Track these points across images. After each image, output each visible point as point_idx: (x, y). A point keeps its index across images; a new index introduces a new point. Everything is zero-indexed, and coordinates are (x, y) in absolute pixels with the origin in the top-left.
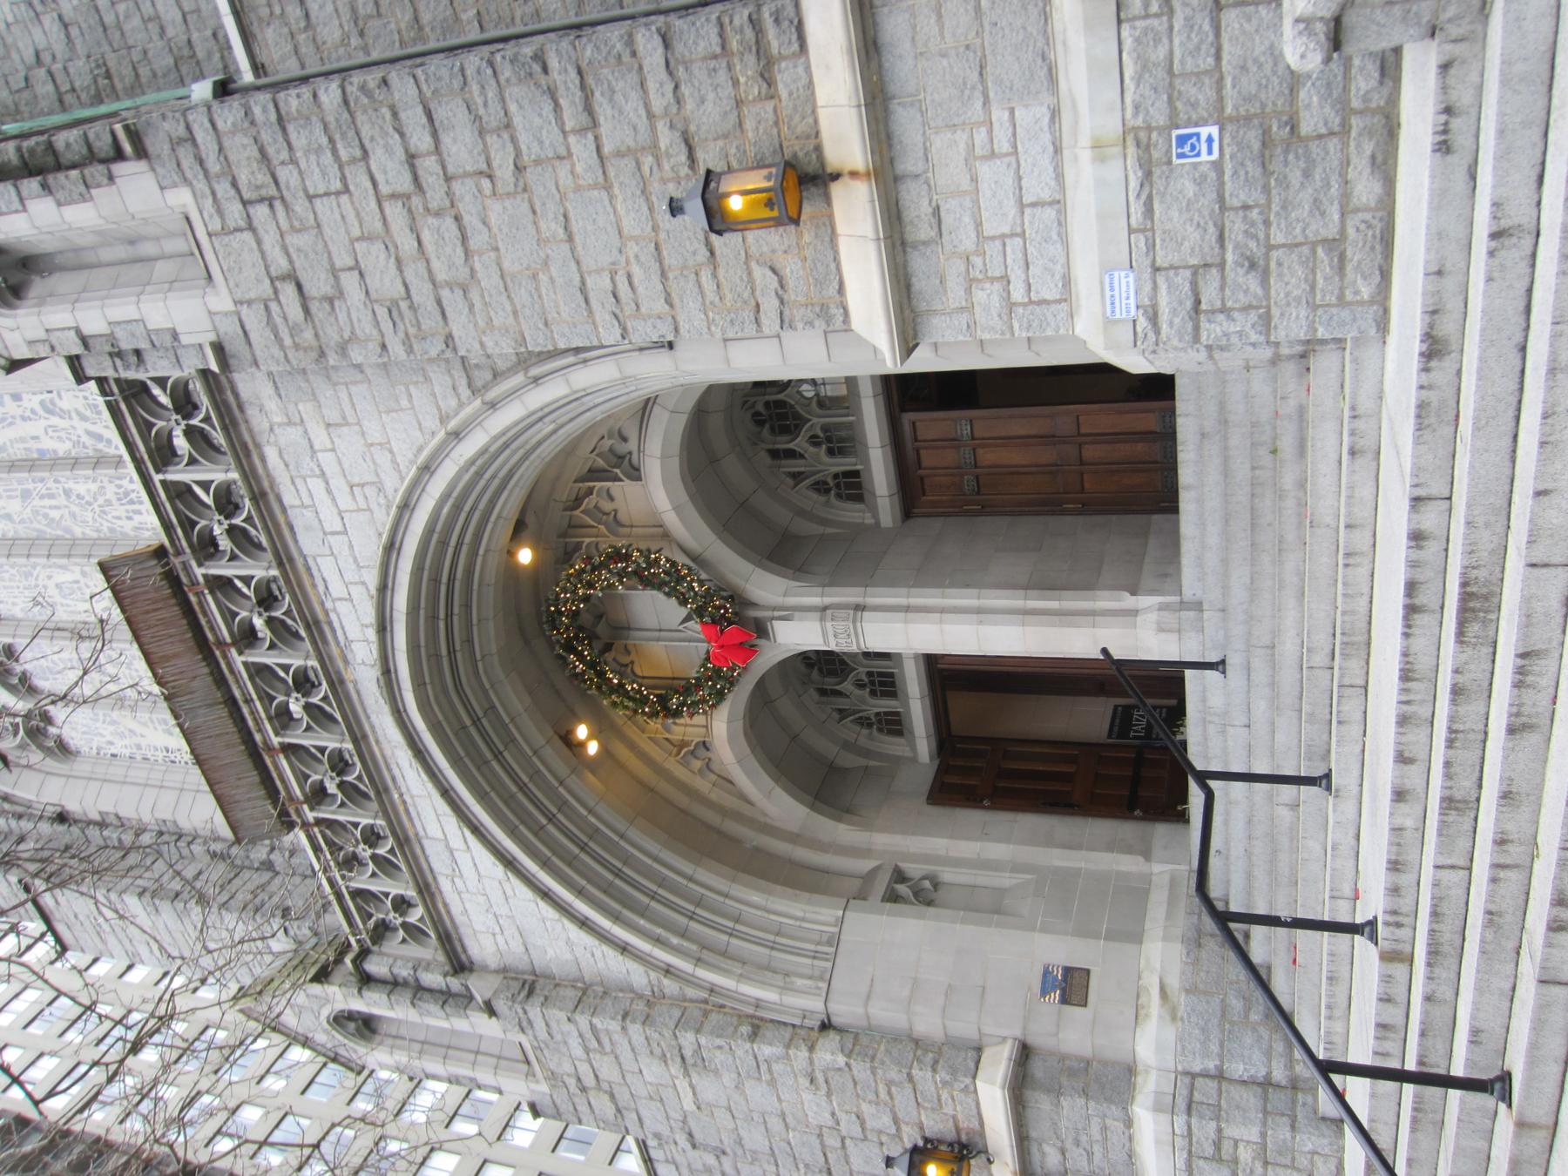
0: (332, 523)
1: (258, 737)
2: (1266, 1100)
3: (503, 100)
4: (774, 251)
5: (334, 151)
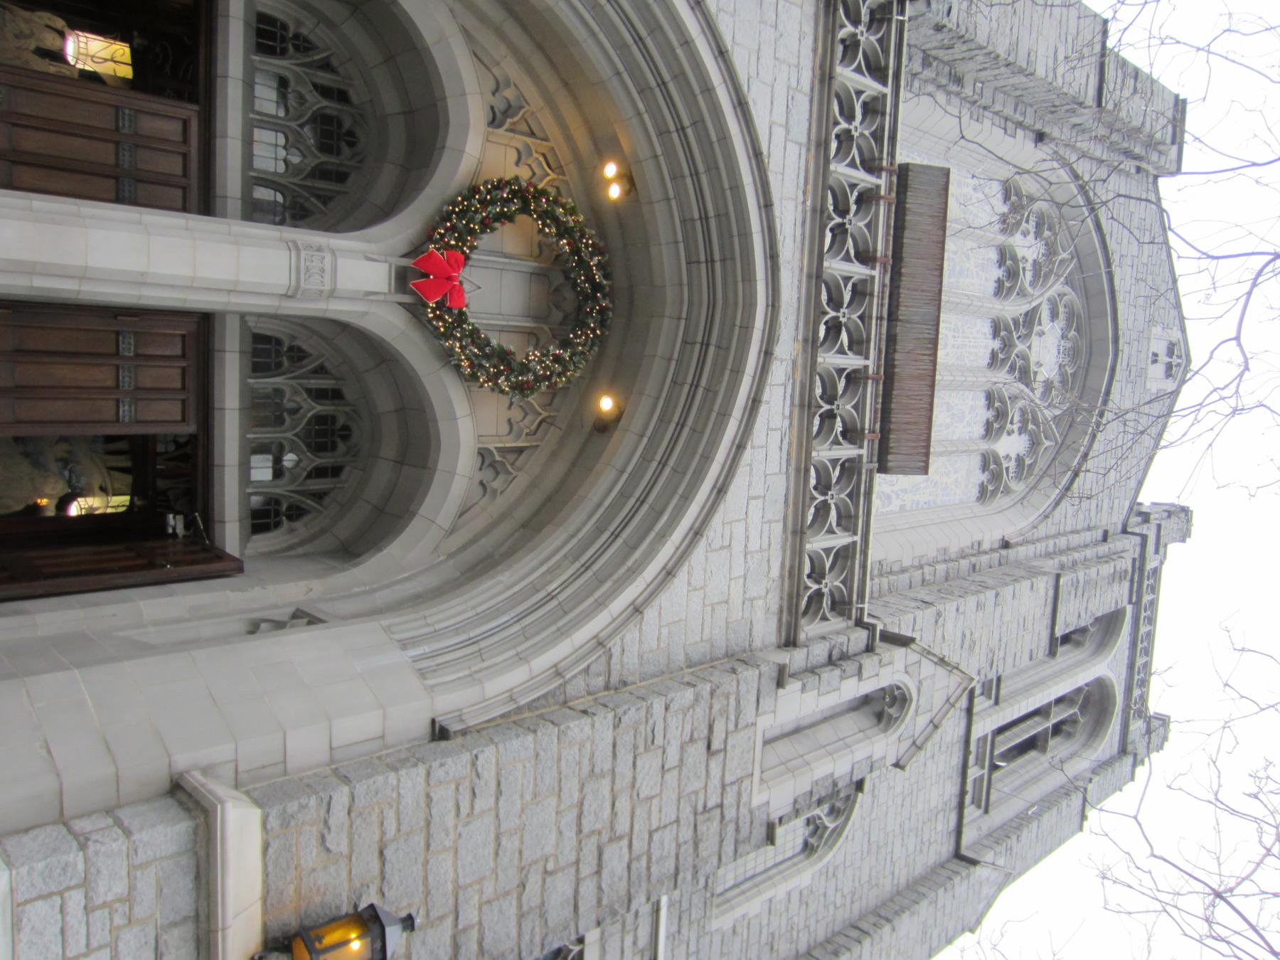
1: (887, 281)
4: (325, 868)
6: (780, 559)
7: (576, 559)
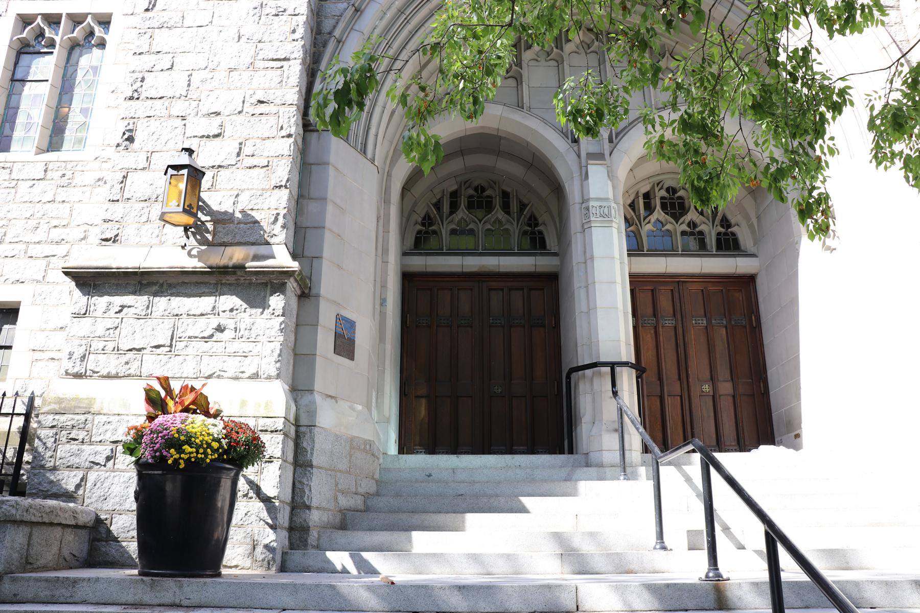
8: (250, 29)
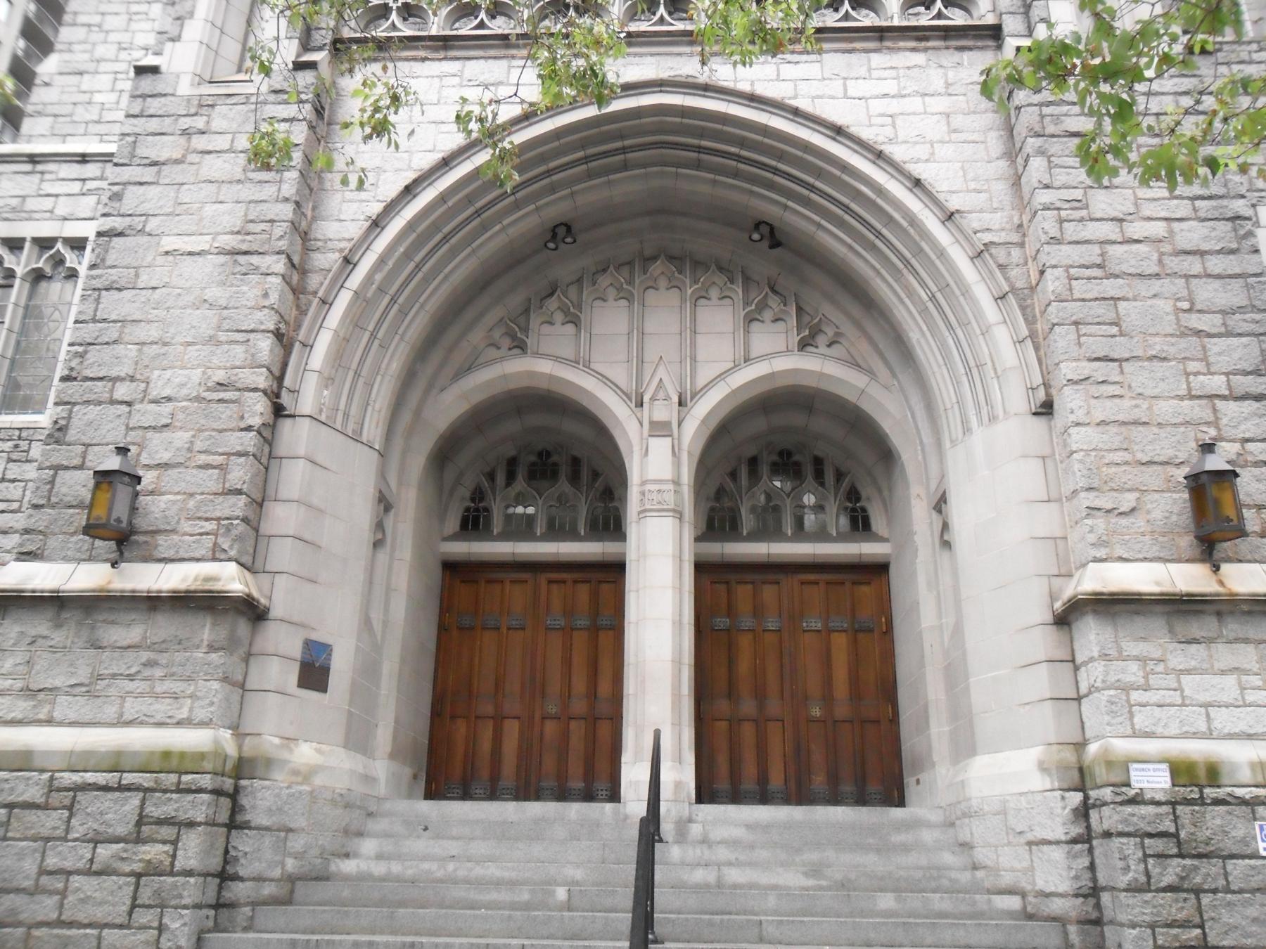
0: (855, 88)
2: (213, 875)
3: (1248, 335)
5: (1202, 198)
6: (908, 54)
7: (899, 271)
8: (214, 293)
